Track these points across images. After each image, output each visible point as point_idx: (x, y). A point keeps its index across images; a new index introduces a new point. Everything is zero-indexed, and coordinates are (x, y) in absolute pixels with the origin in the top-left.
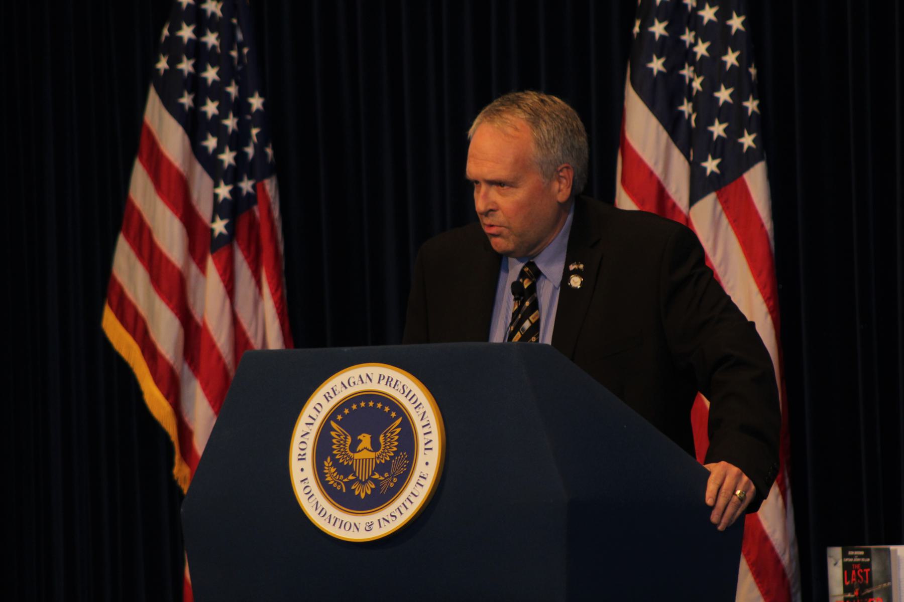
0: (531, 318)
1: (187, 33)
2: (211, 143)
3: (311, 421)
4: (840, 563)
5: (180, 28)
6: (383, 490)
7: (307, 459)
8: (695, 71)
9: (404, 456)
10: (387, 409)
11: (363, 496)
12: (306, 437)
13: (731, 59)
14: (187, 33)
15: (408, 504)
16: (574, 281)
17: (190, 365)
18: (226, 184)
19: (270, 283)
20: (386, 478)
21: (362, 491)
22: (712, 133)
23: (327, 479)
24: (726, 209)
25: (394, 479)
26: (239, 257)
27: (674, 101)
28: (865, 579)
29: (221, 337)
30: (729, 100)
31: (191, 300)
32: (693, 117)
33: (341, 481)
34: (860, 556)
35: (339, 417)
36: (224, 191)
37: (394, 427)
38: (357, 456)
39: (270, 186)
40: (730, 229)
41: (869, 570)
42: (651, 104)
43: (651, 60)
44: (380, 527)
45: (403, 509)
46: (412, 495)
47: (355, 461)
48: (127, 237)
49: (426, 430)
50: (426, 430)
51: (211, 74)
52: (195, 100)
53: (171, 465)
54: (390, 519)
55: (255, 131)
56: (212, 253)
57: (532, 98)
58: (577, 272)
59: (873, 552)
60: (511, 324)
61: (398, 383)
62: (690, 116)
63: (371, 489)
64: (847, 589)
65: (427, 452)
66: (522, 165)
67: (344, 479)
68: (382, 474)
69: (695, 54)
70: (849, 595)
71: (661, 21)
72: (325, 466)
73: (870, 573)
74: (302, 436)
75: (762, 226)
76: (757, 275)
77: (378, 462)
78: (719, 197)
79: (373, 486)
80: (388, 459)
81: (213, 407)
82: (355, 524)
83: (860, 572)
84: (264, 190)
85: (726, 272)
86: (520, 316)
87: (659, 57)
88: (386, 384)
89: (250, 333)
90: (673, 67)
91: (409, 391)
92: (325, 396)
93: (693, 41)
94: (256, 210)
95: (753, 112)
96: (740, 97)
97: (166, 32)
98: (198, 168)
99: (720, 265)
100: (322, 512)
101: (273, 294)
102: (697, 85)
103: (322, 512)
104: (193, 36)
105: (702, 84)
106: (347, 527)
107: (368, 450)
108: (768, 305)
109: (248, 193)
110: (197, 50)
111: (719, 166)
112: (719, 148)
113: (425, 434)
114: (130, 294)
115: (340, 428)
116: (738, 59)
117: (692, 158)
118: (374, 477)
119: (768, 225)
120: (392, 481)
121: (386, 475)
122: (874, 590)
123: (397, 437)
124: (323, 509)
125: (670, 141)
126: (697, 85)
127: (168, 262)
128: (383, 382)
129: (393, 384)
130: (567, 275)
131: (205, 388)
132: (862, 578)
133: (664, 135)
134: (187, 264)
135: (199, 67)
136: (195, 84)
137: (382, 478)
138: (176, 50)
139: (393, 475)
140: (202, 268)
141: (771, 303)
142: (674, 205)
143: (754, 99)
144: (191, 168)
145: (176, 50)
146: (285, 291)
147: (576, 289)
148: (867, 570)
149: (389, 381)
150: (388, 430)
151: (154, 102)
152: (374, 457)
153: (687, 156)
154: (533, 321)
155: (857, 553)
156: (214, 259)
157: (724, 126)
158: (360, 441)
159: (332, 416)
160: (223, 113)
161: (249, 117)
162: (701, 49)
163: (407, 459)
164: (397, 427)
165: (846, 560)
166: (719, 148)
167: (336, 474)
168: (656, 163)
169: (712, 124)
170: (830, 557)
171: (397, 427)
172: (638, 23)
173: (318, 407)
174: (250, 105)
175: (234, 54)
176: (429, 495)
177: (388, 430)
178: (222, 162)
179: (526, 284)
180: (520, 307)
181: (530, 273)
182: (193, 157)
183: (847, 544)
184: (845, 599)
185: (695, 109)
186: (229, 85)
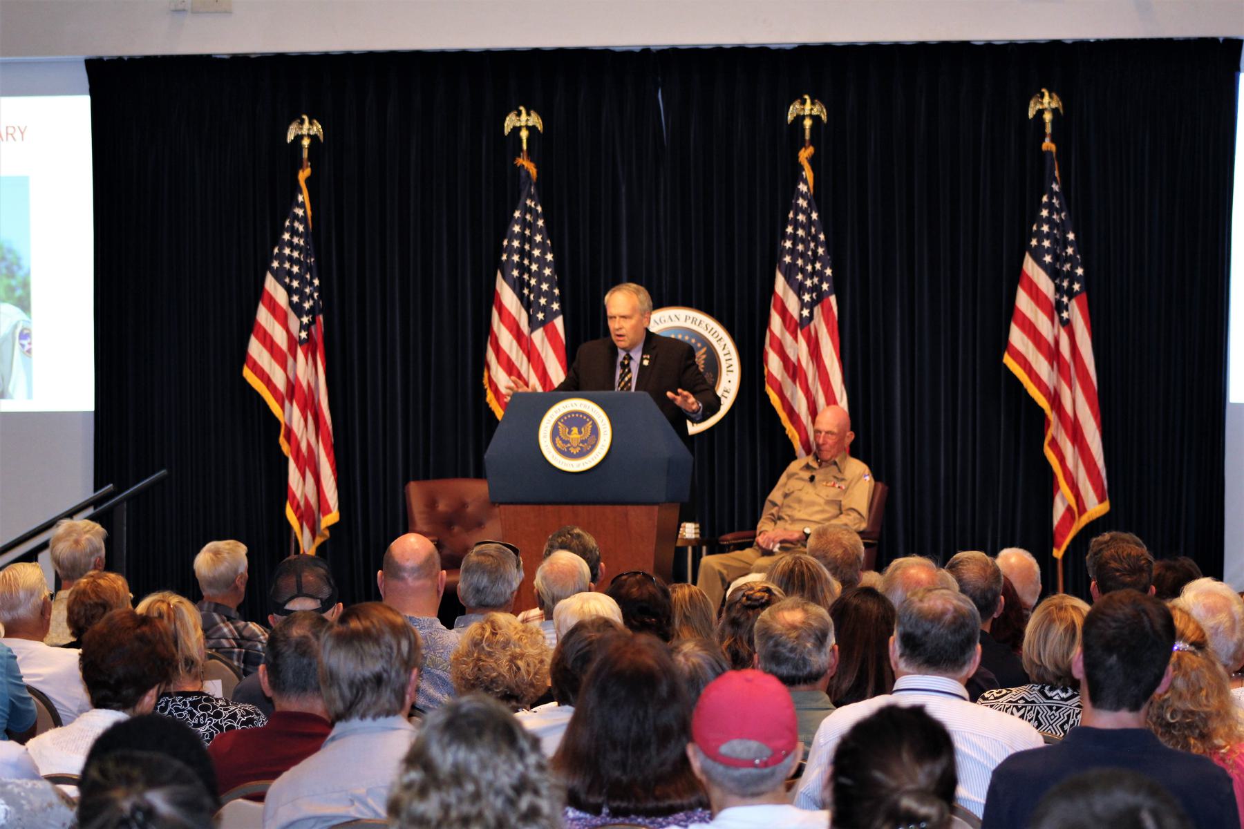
6: (585, 450)
11: (575, 453)
30: (547, 289)
35: (562, 420)
49: (728, 357)
50: (728, 357)
57: (634, 285)
58: (646, 359)
66: (634, 310)
68: (583, 444)
112: (544, 309)
130: (642, 359)
133: (519, 303)
149: (694, 321)
153: (528, 312)
159: (559, 420)
166: (544, 309)
178: (304, 307)
179: (626, 362)
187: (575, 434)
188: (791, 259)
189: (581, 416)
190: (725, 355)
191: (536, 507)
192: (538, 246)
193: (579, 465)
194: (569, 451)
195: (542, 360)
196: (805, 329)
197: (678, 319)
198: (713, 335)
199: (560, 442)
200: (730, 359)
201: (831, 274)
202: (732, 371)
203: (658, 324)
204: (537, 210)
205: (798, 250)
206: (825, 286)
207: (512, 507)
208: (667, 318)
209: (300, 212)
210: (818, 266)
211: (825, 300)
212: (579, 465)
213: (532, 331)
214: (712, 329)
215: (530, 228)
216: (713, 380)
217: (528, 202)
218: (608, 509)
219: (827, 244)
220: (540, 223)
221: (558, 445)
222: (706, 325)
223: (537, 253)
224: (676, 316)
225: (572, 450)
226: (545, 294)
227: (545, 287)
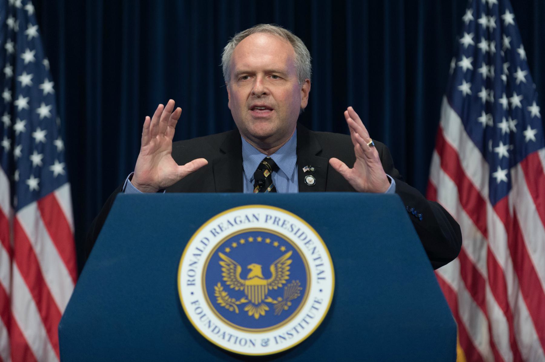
6: (278, 312)
20: (279, 302)
35: (228, 250)
38: (248, 283)
49: (318, 262)
50: (318, 262)
54: (287, 336)
68: (275, 298)
120: (286, 304)
121: (280, 299)
123: (288, 268)
137: (275, 302)
149: (276, 221)
159: (221, 248)
173: (205, 241)
181: (269, 167)
188: (471, 89)
190: (315, 259)
192: (28, 68)
193: (266, 343)
196: (500, 204)
197: (257, 219)
198: (299, 237)
199: (224, 294)
200: (321, 265)
201: (538, 114)
202: (323, 278)
203: (232, 225)
204: (26, 12)
205: (481, 74)
206: (530, 134)
210: (516, 100)
211: (530, 157)
212: (266, 343)
214: (299, 230)
215: (14, 40)
216: (301, 289)
219: (529, 65)
220: (32, 31)
222: (292, 226)
223: (25, 79)
224: (254, 216)
225: (250, 311)
226: (42, 148)
227: (39, 135)
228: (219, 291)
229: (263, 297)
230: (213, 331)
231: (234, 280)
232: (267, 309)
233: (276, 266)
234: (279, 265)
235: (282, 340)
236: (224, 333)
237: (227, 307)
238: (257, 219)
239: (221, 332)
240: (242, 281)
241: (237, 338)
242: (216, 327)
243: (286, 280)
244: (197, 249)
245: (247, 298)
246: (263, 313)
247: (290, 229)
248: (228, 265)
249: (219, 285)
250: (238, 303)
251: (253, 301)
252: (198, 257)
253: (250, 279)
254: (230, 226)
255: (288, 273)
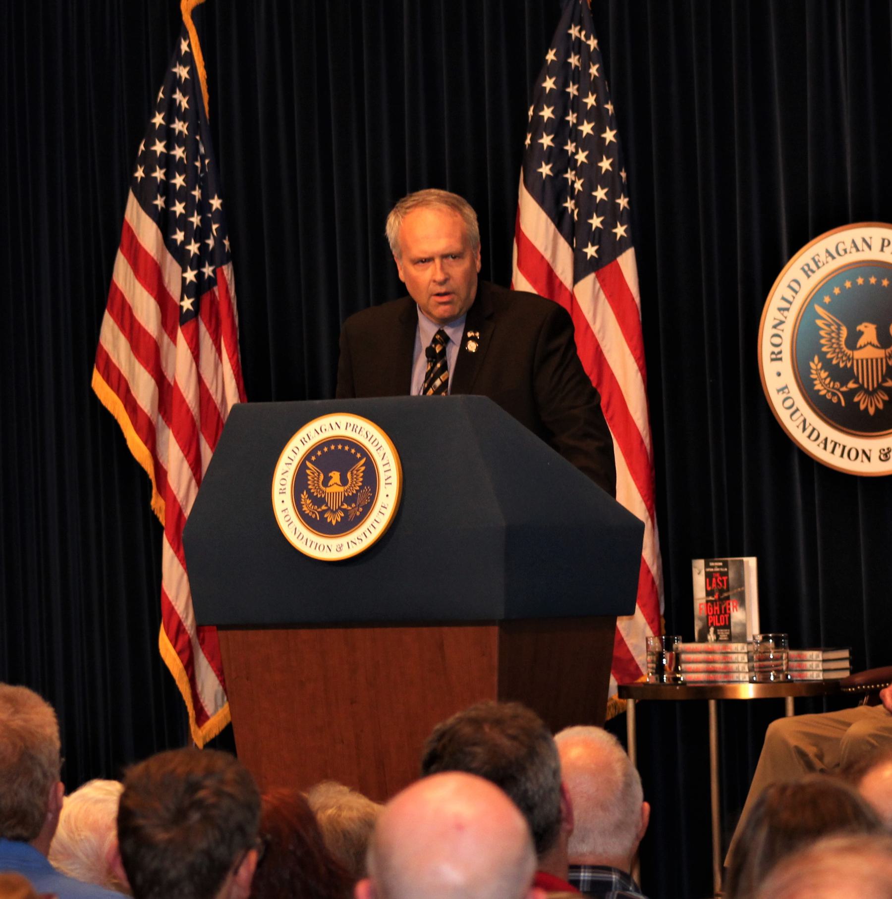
0: (441, 377)
1: (159, 147)
2: (180, 236)
3: (290, 461)
4: (703, 573)
5: (154, 144)
6: (351, 517)
7: (286, 493)
8: (576, 175)
9: (368, 490)
10: (353, 451)
11: (334, 523)
12: (286, 474)
13: (605, 164)
14: (159, 147)
15: (372, 529)
16: (470, 345)
17: (163, 417)
18: (192, 270)
19: (227, 350)
20: (353, 508)
21: (333, 519)
22: (591, 225)
23: (304, 509)
24: (603, 286)
25: (360, 508)
26: (203, 328)
27: (559, 199)
28: (723, 584)
29: (190, 394)
31: (164, 364)
32: (576, 212)
33: (316, 510)
34: (719, 567)
35: (313, 458)
36: (190, 275)
37: (359, 466)
38: (328, 490)
39: (227, 271)
40: (606, 302)
41: (726, 577)
42: (541, 202)
43: (541, 166)
44: (349, 547)
45: (368, 533)
46: (375, 522)
47: (327, 494)
48: (111, 314)
49: (387, 468)
50: (387, 468)
51: (179, 181)
52: (166, 202)
53: (150, 497)
54: (357, 541)
55: (215, 227)
56: (182, 324)
58: (473, 339)
59: (730, 563)
60: (425, 382)
61: (362, 429)
62: (573, 211)
63: (341, 517)
64: (708, 593)
65: (387, 486)
67: (318, 508)
68: (349, 505)
69: (576, 161)
70: (711, 598)
71: (548, 135)
72: (301, 498)
73: (728, 581)
74: (283, 474)
75: (633, 299)
76: (629, 340)
77: (346, 495)
78: (597, 277)
79: (343, 515)
80: (355, 492)
81: (183, 451)
82: (328, 546)
83: (720, 580)
84: (223, 274)
85: (603, 338)
86: (432, 375)
87: (547, 164)
88: (353, 430)
89: (212, 391)
90: (558, 172)
91: (371, 436)
92: (301, 441)
93: (574, 151)
94: (216, 289)
95: (624, 207)
96: (612, 195)
97: (142, 147)
98: (169, 256)
99: (599, 331)
100: (300, 536)
101: (230, 359)
102: (578, 186)
103: (300, 536)
104: (164, 150)
105: (582, 185)
106: (322, 548)
107: (338, 485)
108: (638, 364)
109: (209, 277)
110: (167, 162)
111: (597, 251)
112: (597, 237)
113: (385, 471)
114: (114, 360)
115: (316, 468)
116: (611, 165)
117: (575, 245)
118: (343, 507)
119: (637, 300)
120: (358, 510)
121: (353, 505)
122: (730, 593)
123: (362, 474)
124: (301, 533)
125: (557, 231)
126: (578, 186)
127: (146, 333)
128: (350, 429)
129: (358, 430)
130: (465, 340)
131: (177, 436)
132: (721, 584)
133: (552, 227)
134: (161, 335)
135: (169, 175)
136: (166, 189)
137: (349, 508)
138: (150, 162)
139: (358, 506)
140: (174, 339)
141: (641, 363)
142: (561, 284)
143: (625, 197)
144: (163, 257)
145: (150, 162)
146: (240, 356)
147: (472, 352)
148: (725, 578)
149: (354, 429)
150: (354, 469)
151: (132, 202)
152: (343, 490)
153: (571, 244)
154: (443, 380)
155: (716, 564)
156: (182, 331)
157: (601, 219)
158: (331, 477)
159: (307, 457)
160: (189, 212)
161: (210, 215)
162: (581, 157)
163: (370, 492)
164: (362, 466)
165: (708, 570)
166: (597, 237)
167: (311, 505)
168: (546, 249)
169: (592, 218)
170: (695, 567)
171: (362, 466)
172: (529, 136)
173: (296, 450)
174: (211, 205)
175: (198, 164)
176: (389, 523)
177: (354, 469)
178: (189, 251)
179: (438, 349)
180: (432, 368)
181: (441, 340)
182: (165, 247)
183: (708, 556)
184: (707, 602)
185: (576, 205)
186: (194, 189)
187: (335, 488)
189: (347, 448)
191: (282, 633)
193: (340, 549)
194: (324, 519)
195: (593, 335)
199: (309, 501)
207: (239, 633)
208: (328, 427)
209: (182, 72)
212: (340, 549)
213: (576, 279)
217: (574, 31)
218: (409, 635)
221: (305, 508)
224: (864, 240)
225: (863, 402)
228: (816, 370)
229: (880, 380)
230: (809, 437)
231: (837, 350)
232: (886, 398)
233: (352, 473)
234: (355, 472)
235: (354, 545)
236: (826, 440)
237: (829, 396)
238: (870, 247)
239: (822, 438)
240: (849, 352)
241: (844, 447)
242: (814, 429)
243: (359, 486)
244: (783, 299)
245: (327, 505)
246: (881, 406)
247: (366, 436)
248: (829, 325)
249: (816, 359)
250: (844, 389)
251: (866, 386)
252: (786, 313)
253: (861, 348)
254: (830, 259)
255: (361, 479)
